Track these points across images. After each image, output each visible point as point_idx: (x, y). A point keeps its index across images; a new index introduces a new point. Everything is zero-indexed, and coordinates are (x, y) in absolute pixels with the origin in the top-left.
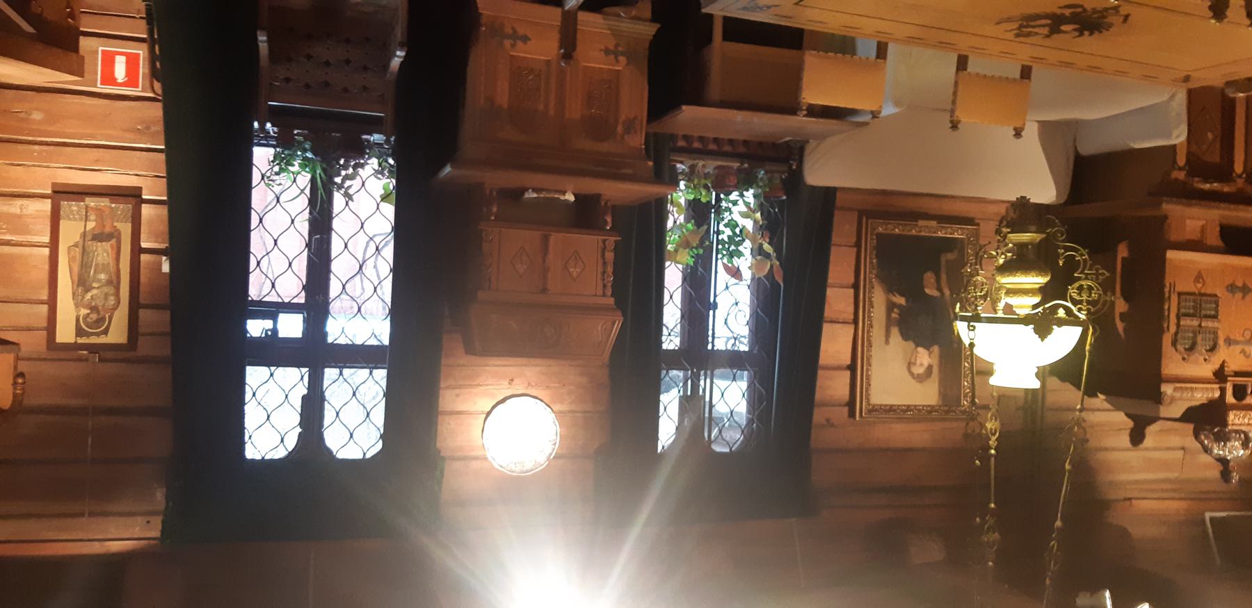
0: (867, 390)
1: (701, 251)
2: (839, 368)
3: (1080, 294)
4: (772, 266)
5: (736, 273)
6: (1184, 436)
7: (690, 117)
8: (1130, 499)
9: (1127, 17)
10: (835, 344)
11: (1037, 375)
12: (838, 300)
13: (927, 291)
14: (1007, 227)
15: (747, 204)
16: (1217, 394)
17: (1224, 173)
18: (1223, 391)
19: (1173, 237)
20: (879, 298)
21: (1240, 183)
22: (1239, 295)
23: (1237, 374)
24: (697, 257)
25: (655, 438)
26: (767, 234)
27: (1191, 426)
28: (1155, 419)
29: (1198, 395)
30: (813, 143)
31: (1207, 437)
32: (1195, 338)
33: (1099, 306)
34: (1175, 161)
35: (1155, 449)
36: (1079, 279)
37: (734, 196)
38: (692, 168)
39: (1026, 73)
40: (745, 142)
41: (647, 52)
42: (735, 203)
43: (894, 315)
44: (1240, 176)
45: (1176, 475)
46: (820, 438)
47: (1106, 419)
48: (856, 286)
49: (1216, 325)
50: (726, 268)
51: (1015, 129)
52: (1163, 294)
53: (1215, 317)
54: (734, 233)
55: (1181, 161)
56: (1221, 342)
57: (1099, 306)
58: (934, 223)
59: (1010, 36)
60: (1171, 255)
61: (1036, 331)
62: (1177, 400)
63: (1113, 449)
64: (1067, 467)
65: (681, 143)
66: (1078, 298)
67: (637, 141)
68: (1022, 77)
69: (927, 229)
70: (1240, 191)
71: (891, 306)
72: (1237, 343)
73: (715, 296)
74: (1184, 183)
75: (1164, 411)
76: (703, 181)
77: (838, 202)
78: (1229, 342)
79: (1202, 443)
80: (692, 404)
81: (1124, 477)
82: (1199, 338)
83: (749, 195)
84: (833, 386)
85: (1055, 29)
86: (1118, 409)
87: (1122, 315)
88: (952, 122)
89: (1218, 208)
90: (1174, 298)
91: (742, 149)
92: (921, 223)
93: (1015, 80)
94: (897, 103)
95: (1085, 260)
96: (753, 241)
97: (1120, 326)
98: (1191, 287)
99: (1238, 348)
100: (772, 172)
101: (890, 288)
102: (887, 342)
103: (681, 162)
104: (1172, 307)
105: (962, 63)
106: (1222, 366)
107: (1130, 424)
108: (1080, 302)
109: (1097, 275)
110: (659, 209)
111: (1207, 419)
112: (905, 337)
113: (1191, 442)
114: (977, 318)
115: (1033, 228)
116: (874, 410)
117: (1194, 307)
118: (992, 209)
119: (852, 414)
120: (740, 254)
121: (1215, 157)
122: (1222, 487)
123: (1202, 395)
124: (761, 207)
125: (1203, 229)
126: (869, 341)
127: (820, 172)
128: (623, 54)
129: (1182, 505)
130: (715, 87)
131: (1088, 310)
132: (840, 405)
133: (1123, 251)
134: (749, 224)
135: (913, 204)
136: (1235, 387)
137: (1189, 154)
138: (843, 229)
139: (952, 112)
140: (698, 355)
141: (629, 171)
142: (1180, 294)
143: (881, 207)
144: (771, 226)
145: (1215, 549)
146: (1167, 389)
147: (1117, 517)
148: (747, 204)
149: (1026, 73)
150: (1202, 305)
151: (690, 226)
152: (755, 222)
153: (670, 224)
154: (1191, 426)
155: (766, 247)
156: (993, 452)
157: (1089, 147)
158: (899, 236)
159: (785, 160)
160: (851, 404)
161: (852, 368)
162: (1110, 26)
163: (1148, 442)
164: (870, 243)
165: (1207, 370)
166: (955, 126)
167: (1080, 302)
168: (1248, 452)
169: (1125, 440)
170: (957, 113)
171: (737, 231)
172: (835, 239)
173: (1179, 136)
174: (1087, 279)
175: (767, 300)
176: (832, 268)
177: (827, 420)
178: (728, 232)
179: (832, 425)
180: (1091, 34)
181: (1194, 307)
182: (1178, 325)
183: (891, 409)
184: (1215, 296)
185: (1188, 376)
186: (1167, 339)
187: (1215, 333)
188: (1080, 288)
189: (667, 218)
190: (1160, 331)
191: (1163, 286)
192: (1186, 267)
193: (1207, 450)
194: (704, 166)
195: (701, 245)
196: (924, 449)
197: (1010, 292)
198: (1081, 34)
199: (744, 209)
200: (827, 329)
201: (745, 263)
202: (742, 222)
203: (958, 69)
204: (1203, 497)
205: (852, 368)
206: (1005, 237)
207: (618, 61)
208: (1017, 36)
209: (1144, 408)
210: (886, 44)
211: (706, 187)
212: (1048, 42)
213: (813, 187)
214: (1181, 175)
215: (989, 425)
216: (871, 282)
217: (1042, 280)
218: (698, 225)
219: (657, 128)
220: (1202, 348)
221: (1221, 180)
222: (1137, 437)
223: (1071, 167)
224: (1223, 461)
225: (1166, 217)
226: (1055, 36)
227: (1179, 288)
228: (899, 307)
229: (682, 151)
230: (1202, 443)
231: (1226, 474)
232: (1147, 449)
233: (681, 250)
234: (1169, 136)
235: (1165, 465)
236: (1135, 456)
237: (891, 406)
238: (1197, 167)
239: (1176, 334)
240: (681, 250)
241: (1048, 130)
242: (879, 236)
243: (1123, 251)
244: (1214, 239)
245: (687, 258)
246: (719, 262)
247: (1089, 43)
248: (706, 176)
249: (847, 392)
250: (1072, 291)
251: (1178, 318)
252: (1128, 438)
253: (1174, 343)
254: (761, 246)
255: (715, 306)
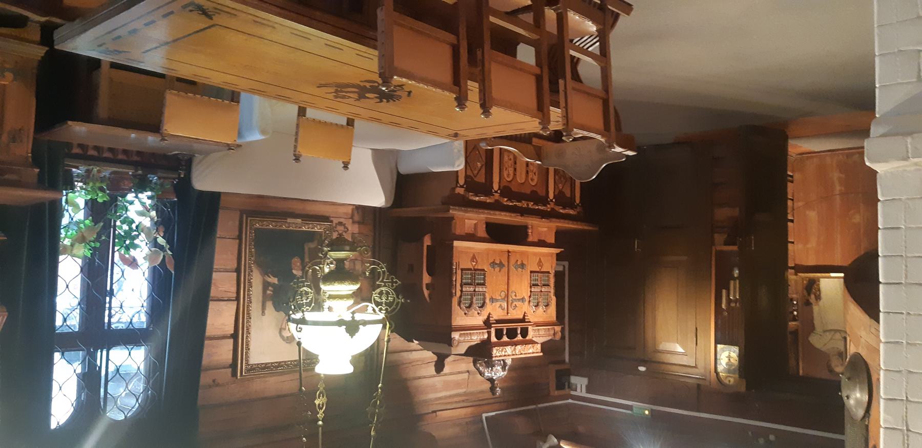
0: (247, 353)
1: (98, 245)
2: (224, 337)
3: (380, 298)
4: (164, 256)
5: (133, 263)
6: (467, 364)
7: (79, 130)
8: (435, 412)
9: (410, 92)
10: (220, 318)
11: (351, 362)
12: (223, 282)
13: (294, 272)
14: (328, 246)
15: (143, 204)
16: (486, 336)
17: (488, 191)
18: (489, 333)
19: (458, 231)
20: (257, 280)
21: (497, 196)
22: (497, 269)
23: (498, 322)
24: (94, 249)
25: (47, 414)
26: (162, 229)
27: (471, 359)
28: (448, 356)
29: (474, 338)
30: (198, 157)
31: (481, 365)
32: (472, 299)
33: (394, 306)
34: (457, 182)
35: (451, 374)
36: (379, 286)
37: (130, 197)
38: (88, 171)
39: (350, 123)
40: (139, 153)
41: (35, 71)
42: (131, 203)
43: (269, 292)
44: (496, 192)
45: (464, 390)
46: (204, 397)
47: (420, 356)
48: (238, 271)
49: (484, 289)
50: (122, 258)
51: (343, 162)
52: (451, 269)
53: (483, 284)
54: (131, 229)
55: (462, 181)
56: (487, 301)
57: (394, 306)
58: (299, 221)
59: (331, 96)
60: (456, 243)
61: (348, 330)
62: (462, 342)
63: (425, 377)
64: (373, 433)
65: (76, 150)
66: (379, 300)
67: (24, 149)
68: (348, 124)
69: (294, 224)
70: (497, 201)
71: (266, 285)
72: (497, 300)
73: (112, 284)
74: (463, 196)
75: (454, 351)
76: (98, 185)
77: (222, 203)
78: (492, 300)
79: (478, 369)
80: (91, 381)
81: (432, 396)
82: (475, 298)
83: (145, 196)
84: (218, 353)
85: (361, 96)
86: (426, 348)
87: (427, 284)
88: (295, 155)
89: (483, 213)
90: (459, 272)
91: (135, 158)
92: (289, 220)
93: (342, 126)
94: (263, 132)
95: (384, 272)
96: (148, 236)
97: (426, 293)
98: (469, 265)
99: (498, 304)
100: (164, 178)
101: (265, 273)
102: (263, 313)
103: (77, 168)
104: (457, 278)
105: (302, 112)
106: (489, 317)
107: (435, 358)
108: (381, 304)
109: (392, 282)
110: (55, 211)
111: (480, 353)
112: (277, 308)
113: (471, 367)
114: (303, 321)
115: (348, 248)
116: (253, 369)
117: (471, 279)
118: (342, 210)
119: (234, 374)
120: (135, 247)
121: (481, 178)
122: (489, 395)
123: (477, 338)
124: (155, 207)
125: (476, 225)
126: (248, 314)
127: (205, 180)
128: (9, 70)
129: (469, 410)
130: (103, 106)
131: (386, 309)
132: (224, 368)
133: (427, 241)
134: (147, 222)
135: (282, 206)
136: (497, 331)
137: (466, 177)
138: (226, 225)
139: (295, 147)
140: (96, 334)
141: (13, 177)
142: (462, 270)
143: (258, 208)
144: (164, 222)
145: (488, 437)
146: (456, 335)
147: (430, 427)
148: (143, 204)
149: (350, 123)
150: (476, 277)
151: (87, 222)
152: (152, 219)
153: (65, 221)
154: (471, 359)
155: (161, 240)
156: (320, 423)
157: (406, 168)
158: (271, 230)
159: (175, 169)
160: (234, 365)
161: (235, 336)
162: (400, 97)
163: (446, 370)
164: (248, 236)
165: (479, 320)
166: (297, 159)
167: (381, 304)
168: (506, 373)
169: (432, 370)
170: (299, 149)
171: (134, 226)
172: (219, 233)
173: (459, 165)
174: (385, 286)
175: (161, 285)
176: (217, 257)
177: (214, 381)
178: (125, 227)
179: (218, 385)
180: (388, 101)
181: (471, 279)
182: (462, 291)
183: (265, 367)
184: (483, 270)
185: (469, 323)
186: (455, 301)
187: (484, 295)
188: (381, 293)
189: (62, 216)
190: (451, 296)
191: (452, 264)
192: (465, 251)
193: (481, 374)
194: (99, 171)
195: (97, 240)
196: (292, 395)
197: (331, 297)
198: (381, 101)
199: (141, 208)
200: (212, 306)
201: (142, 251)
202: (138, 219)
203: (299, 115)
204: (479, 404)
205: (235, 336)
206: (326, 254)
207: (4, 77)
208: (336, 97)
209: (442, 348)
210: (239, 93)
211: (101, 189)
212: (357, 103)
213: (202, 193)
214: (460, 191)
215: (317, 402)
216: (250, 267)
217: (355, 287)
218: (95, 221)
219: (46, 137)
220: (475, 306)
221: (486, 196)
222: (439, 367)
223: (395, 181)
224: (491, 380)
225: (452, 218)
226: (362, 100)
227: (462, 266)
228: (273, 285)
229: (77, 157)
230: (478, 369)
231: (493, 389)
232: (446, 375)
233: (77, 245)
234: (453, 166)
235: (458, 384)
236: (438, 380)
237: (266, 364)
238: (471, 185)
239: (461, 297)
240: (77, 245)
241: (380, 157)
242: (257, 230)
243: (427, 241)
244: (482, 232)
245: (83, 251)
246: (117, 255)
247: (387, 107)
248: (102, 180)
249: (231, 356)
250: (375, 295)
251: (461, 286)
252: (434, 368)
253: (459, 304)
254: (156, 239)
255: (111, 293)
